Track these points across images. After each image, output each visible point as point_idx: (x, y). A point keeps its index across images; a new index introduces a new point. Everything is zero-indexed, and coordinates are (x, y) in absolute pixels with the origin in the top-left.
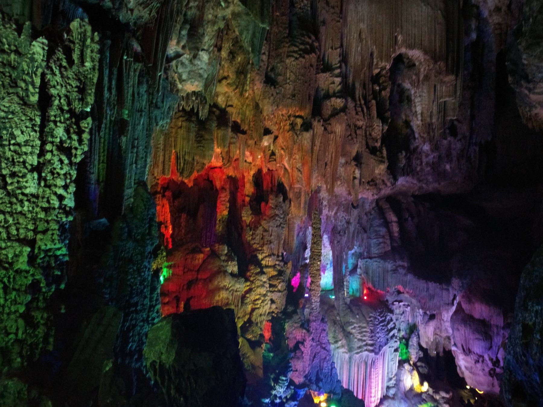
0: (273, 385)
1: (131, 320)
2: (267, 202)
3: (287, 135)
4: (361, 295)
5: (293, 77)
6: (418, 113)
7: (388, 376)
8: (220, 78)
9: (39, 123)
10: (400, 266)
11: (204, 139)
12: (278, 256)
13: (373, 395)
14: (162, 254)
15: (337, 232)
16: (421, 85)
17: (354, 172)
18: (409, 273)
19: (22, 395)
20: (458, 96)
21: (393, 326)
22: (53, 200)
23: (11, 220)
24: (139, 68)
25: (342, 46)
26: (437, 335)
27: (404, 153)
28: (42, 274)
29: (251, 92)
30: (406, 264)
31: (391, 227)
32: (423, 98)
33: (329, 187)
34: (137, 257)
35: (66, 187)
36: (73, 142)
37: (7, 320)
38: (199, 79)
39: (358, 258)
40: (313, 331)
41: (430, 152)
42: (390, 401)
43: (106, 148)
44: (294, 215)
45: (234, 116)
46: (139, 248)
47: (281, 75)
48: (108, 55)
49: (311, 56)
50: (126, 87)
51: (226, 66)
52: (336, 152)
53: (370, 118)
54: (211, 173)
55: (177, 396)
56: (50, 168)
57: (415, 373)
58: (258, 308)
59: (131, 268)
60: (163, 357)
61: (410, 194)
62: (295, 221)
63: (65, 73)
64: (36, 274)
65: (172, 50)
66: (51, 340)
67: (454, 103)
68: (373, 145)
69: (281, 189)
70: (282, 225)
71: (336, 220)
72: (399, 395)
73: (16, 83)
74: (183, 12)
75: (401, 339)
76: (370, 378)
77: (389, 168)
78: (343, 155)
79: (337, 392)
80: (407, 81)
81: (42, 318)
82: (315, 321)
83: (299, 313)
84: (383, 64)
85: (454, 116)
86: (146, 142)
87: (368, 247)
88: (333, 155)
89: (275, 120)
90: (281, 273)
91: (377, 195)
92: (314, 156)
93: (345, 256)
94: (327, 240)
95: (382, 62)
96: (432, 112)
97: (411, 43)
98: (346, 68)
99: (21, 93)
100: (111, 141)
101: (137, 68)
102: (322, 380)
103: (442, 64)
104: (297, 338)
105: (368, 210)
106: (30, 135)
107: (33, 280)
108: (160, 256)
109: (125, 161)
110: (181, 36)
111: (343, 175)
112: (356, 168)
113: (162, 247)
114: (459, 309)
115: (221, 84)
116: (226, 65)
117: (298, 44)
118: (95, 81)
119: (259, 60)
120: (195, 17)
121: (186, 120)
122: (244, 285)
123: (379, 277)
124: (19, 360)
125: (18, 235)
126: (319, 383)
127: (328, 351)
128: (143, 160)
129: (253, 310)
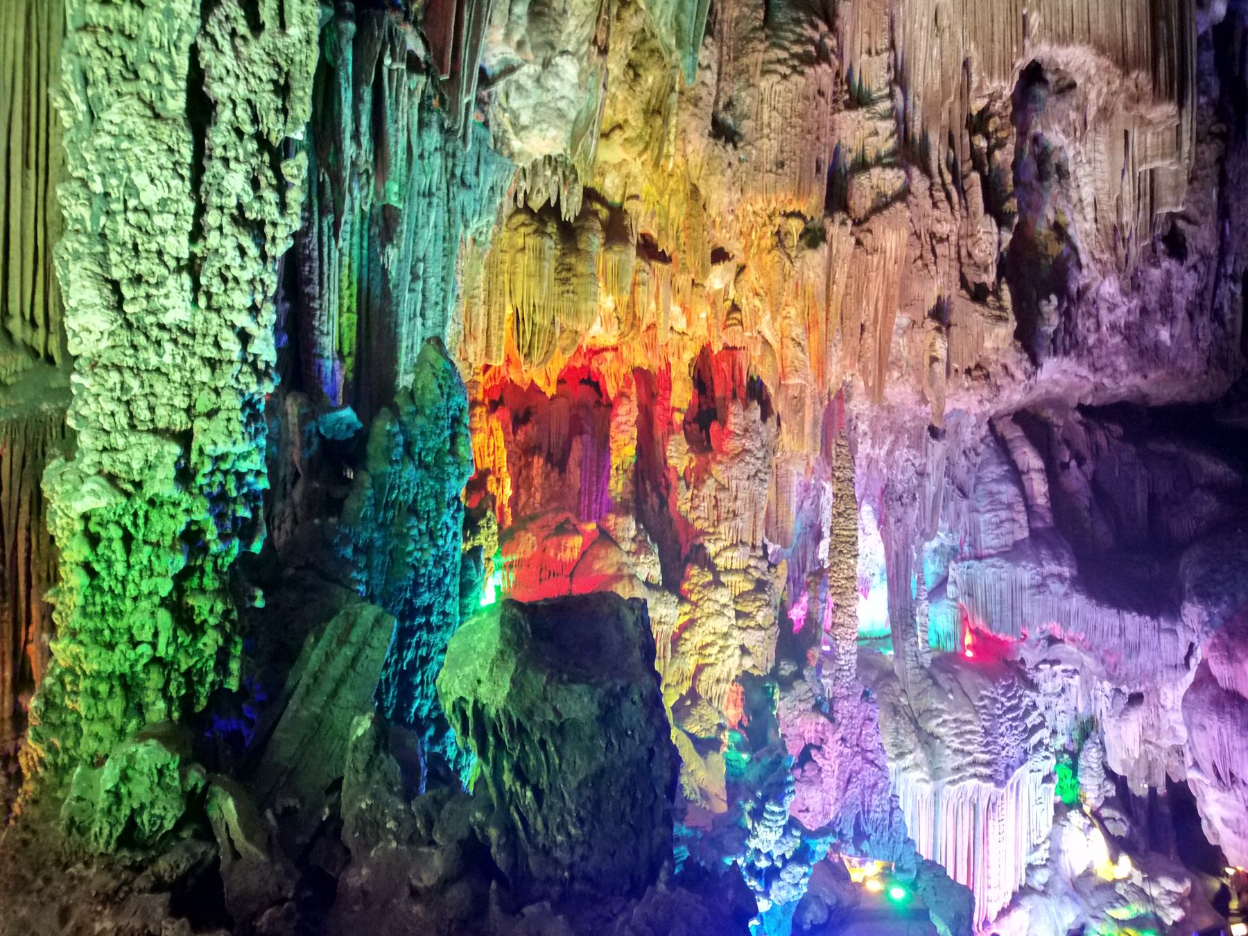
0: (750, 827)
1: (418, 646)
2: (724, 423)
3: (767, 259)
5: (777, 121)
6: (1085, 203)
8: (606, 127)
9: (189, 160)
10: (1052, 575)
11: (575, 275)
12: (754, 547)
13: (992, 882)
14: (489, 528)
16: (1091, 135)
17: (932, 345)
18: (1077, 591)
19: (168, 780)
20: (1185, 155)
22: (226, 340)
23: (134, 383)
24: (421, 87)
25: (892, 46)
26: (1150, 743)
27: (1054, 299)
28: (210, 511)
29: (679, 160)
30: (1067, 572)
31: (1026, 484)
32: (1098, 165)
33: (870, 384)
34: (427, 505)
35: (254, 310)
36: (267, 208)
37: (132, 613)
38: (558, 122)
40: (844, 722)
41: (1119, 299)
42: (1036, 898)
43: (355, 279)
44: (789, 454)
45: (642, 221)
46: (432, 483)
47: (749, 118)
48: (350, 57)
49: (819, 69)
51: (620, 97)
52: (888, 298)
54: (594, 365)
55: (518, 785)
56: (218, 265)
57: (1097, 833)
59: (413, 527)
61: (1074, 404)
62: (791, 468)
63: (243, 49)
64: (194, 509)
65: (494, 56)
66: (234, 666)
67: (1176, 173)
68: (977, 281)
69: (756, 392)
70: (761, 475)
71: (890, 467)
73: (136, 73)
75: (1059, 754)
76: (986, 842)
77: (1018, 335)
78: (904, 306)
79: (906, 867)
80: (1057, 127)
81: (211, 611)
82: (846, 698)
83: (807, 678)
84: (996, 84)
85: (1177, 205)
86: (444, 268)
87: (973, 534)
89: (737, 227)
90: (761, 586)
91: (989, 401)
92: (832, 309)
93: (915, 555)
94: (871, 516)
95: (991, 82)
96: (1119, 199)
97: (1064, 32)
98: (905, 99)
99: (147, 92)
100: (365, 262)
101: (416, 88)
102: (868, 837)
103: (1142, 77)
104: (806, 736)
105: (969, 445)
106: (169, 187)
107: (189, 524)
108: (484, 532)
109: (398, 305)
110: (514, 18)
111: (905, 354)
112: (938, 335)
113: (489, 513)
114: (1205, 678)
115: (610, 142)
116: (621, 93)
117: (787, 44)
118: (312, 68)
119: (694, 65)
121: (535, 232)
122: (678, 612)
123: (1001, 603)
124: (161, 705)
125: (152, 421)
126: (862, 841)
127: (880, 769)
128: (439, 308)
129: (700, 669)
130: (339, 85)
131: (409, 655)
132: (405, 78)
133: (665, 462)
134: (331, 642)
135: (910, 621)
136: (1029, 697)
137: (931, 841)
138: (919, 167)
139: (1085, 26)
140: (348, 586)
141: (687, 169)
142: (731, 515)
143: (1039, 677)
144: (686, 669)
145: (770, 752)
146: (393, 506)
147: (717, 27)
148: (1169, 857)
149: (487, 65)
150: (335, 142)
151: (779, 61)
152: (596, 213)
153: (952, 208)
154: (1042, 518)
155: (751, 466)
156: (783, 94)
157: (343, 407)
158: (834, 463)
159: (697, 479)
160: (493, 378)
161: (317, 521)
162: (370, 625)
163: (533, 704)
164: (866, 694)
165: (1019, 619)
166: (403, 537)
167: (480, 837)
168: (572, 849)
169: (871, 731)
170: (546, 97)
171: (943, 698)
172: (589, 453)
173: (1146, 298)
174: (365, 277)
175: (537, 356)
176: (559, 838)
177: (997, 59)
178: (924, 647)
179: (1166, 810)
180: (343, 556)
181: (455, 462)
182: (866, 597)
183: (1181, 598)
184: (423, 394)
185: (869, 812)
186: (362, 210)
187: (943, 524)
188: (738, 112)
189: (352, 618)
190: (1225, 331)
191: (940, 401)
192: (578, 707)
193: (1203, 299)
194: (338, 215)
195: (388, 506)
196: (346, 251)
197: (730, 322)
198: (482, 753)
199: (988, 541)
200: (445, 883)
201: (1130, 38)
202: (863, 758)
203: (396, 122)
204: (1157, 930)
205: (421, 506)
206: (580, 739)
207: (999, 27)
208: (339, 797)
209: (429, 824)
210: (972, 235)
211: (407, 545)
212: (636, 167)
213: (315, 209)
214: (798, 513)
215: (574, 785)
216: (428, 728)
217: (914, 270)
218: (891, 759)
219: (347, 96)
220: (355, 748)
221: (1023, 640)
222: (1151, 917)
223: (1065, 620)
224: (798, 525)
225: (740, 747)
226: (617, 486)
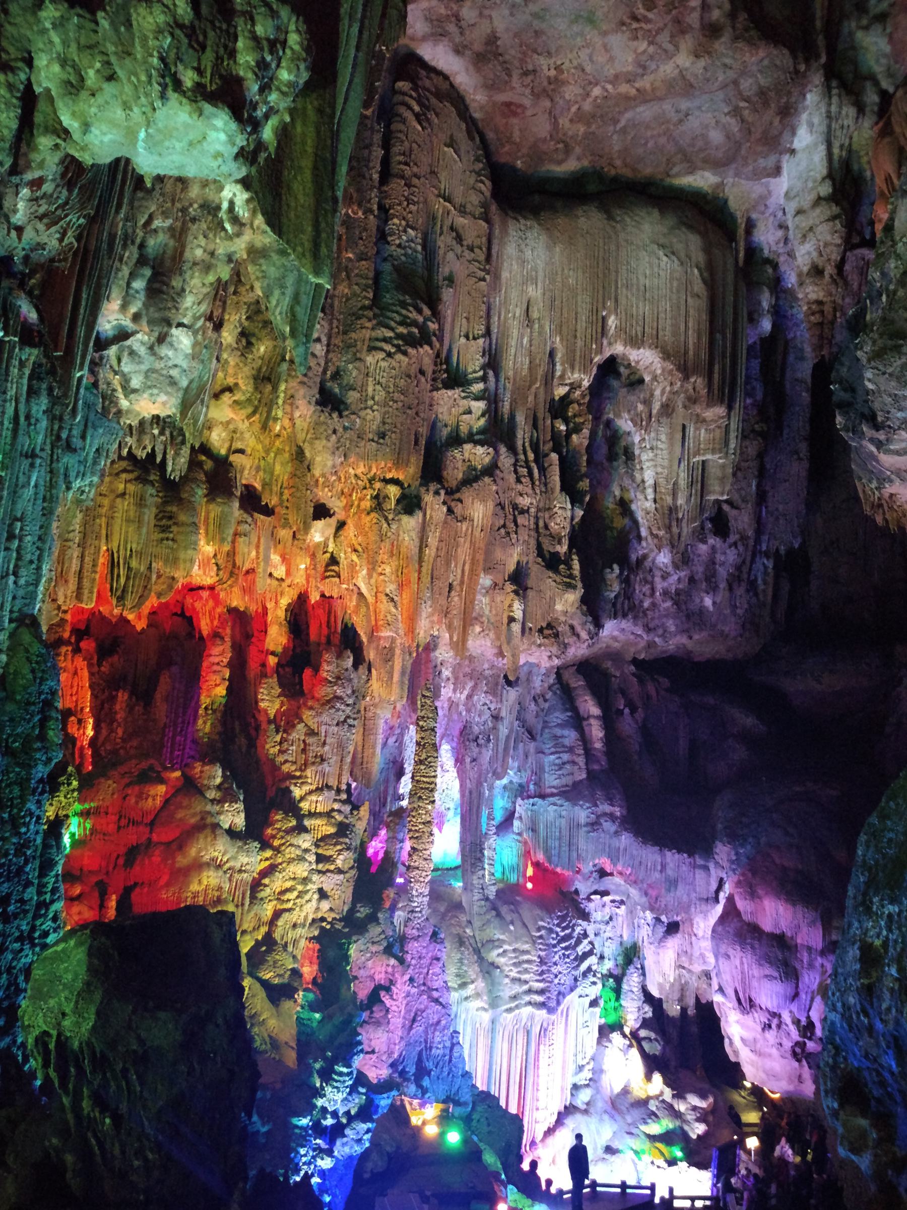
0: (318, 1085)
2: (317, 669)
3: (367, 520)
4: (521, 880)
5: (381, 395)
6: (647, 484)
8: (218, 388)
10: (605, 814)
11: (175, 524)
12: (339, 791)
13: (541, 1105)
14: (69, 784)
16: (654, 424)
17: (510, 606)
18: (626, 830)
21: (588, 948)
24: (33, 358)
25: (488, 333)
26: (684, 968)
29: (287, 423)
30: (617, 811)
31: (586, 729)
34: (11, 792)
38: (169, 389)
39: (516, 797)
41: (670, 569)
42: (578, 1117)
44: (377, 700)
46: (17, 769)
51: (232, 363)
52: (473, 563)
54: (189, 600)
55: (97, 1111)
57: (635, 1053)
60: (67, 1023)
61: (629, 658)
65: (109, 322)
67: (723, 466)
71: (468, 711)
72: (600, 1105)
74: (138, 241)
75: (605, 977)
76: (536, 1066)
77: (584, 600)
78: (488, 570)
79: (462, 1100)
80: (626, 416)
84: (576, 376)
85: (722, 494)
86: (41, 527)
87: (538, 772)
88: (467, 568)
90: (343, 829)
91: (558, 657)
92: (424, 570)
94: (449, 755)
95: (572, 373)
97: (637, 335)
98: (497, 381)
101: (27, 360)
102: (429, 1074)
103: (699, 381)
104: (377, 977)
111: (487, 612)
114: (731, 912)
116: (231, 359)
117: (393, 324)
119: (306, 354)
120: (164, 252)
121: (136, 479)
122: (259, 858)
127: (444, 1007)
128: (34, 566)
129: (277, 914)
132: (17, 350)
135: (479, 855)
136: (581, 926)
138: (506, 446)
141: (294, 432)
142: (318, 760)
143: (591, 907)
144: (263, 915)
148: (695, 1072)
151: (385, 340)
153: (533, 484)
154: (598, 761)
155: (341, 713)
165: (575, 854)
171: (505, 930)
176: (136, 1163)
177: (578, 354)
178: (490, 880)
179: (694, 1029)
181: (44, 747)
182: (440, 830)
183: (714, 838)
184: (14, 679)
185: (431, 1048)
187: (513, 763)
188: (345, 382)
190: (758, 599)
191: (515, 656)
201: (691, 347)
202: (429, 997)
207: (582, 324)
210: (549, 509)
212: (243, 426)
217: (498, 537)
221: (578, 872)
222: (679, 1131)
223: (614, 857)
225: (313, 1007)
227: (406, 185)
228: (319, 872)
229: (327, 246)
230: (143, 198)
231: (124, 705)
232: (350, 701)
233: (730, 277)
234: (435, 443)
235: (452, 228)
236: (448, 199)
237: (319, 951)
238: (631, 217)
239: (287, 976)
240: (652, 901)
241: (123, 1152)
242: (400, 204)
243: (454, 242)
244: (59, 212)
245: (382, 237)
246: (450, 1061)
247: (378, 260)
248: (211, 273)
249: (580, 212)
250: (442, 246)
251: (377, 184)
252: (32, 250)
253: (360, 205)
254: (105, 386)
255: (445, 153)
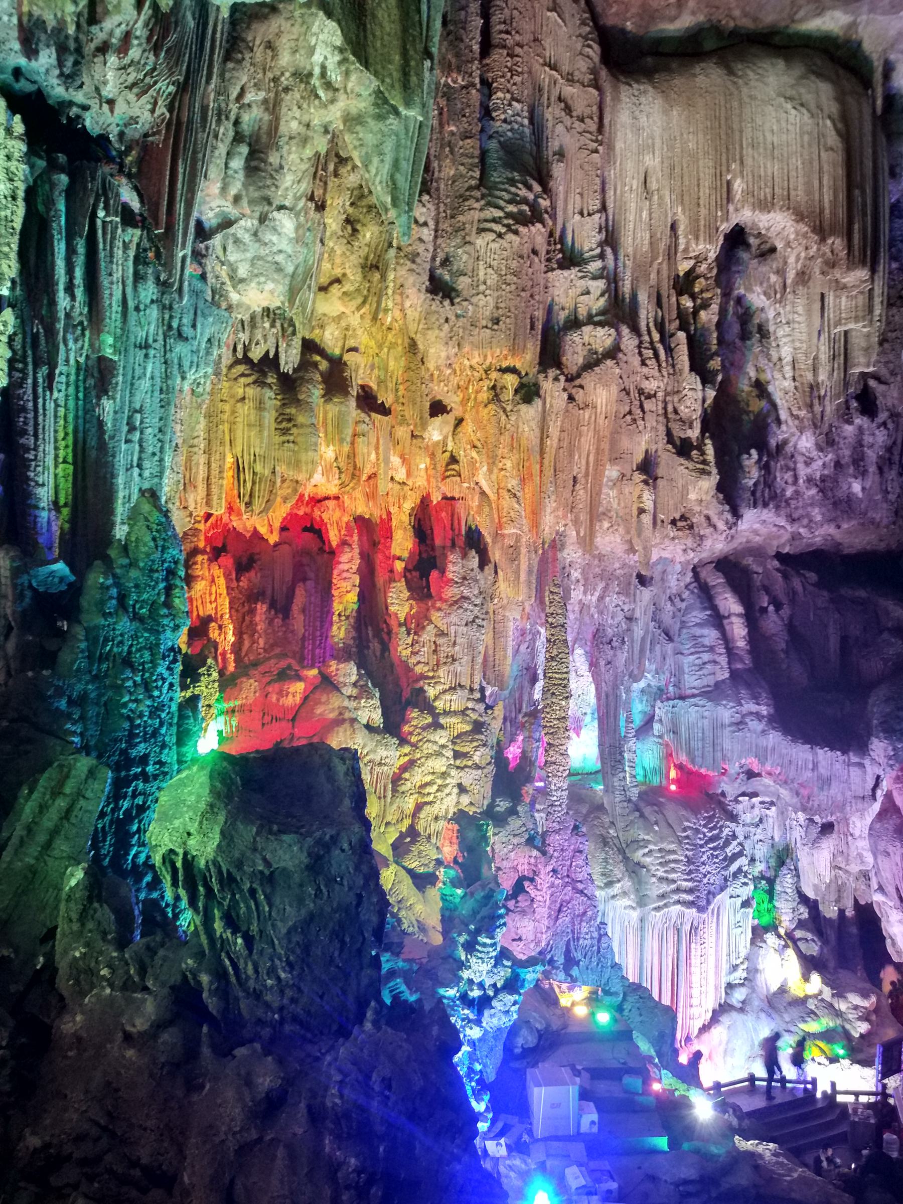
0: (463, 958)
1: (134, 795)
2: (443, 571)
3: (484, 412)
4: (664, 782)
5: (492, 279)
6: (784, 362)
7: (729, 961)
8: (324, 280)
10: (752, 713)
11: (294, 426)
12: (472, 690)
13: (695, 1002)
15: (604, 640)
17: (640, 497)
18: (774, 728)
21: (738, 849)
24: (136, 240)
25: (604, 208)
26: (840, 868)
29: (398, 314)
30: (764, 710)
31: (727, 628)
34: (141, 657)
38: (276, 276)
39: (655, 700)
40: (556, 854)
41: (814, 453)
42: (734, 1014)
43: (70, 429)
44: (505, 601)
46: (146, 635)
50: (106, 283)
51: (339, 252)
52: (598, 451)
53: (675, 373)
54: (317, 513)
57: (791, 953)
58: (430, 803)
59: (128, 679)
60: (192, 842)
65: (212, 209)
67: (868, 335)
68: (683, 436)
71: (601, 613)
72: (756, 1003)
74: (233, 117)
75: (755, 879)
76: (688, 965)
77: (720, 488)
78: (614, 460)
79: (613, 990)
80: (758, 289)
82: (557, 832)
85: (868, 366)
86: (161, 419)
87: (679, 674)
88: (592, 458)
89: (455, 381)
90: (478, 727)
91: (693, 550)
92: (546, 461)
94: (583, 659)
95: (697, 244)
97: (766, 198)
98: (616, 259)
100: (80, 413)
101: (131, 241)
103: (837, 243)
104: (520, 868)
105: (674, 591)
109: (114, 456)
110: (230, 172)
111: (615, 506)
113: (210, 661)
117: (502, 203)
118: (18, 224)
120: (260, 128)
121: (254, 382)
122: (398, 753)
127: (589, 898)
128: (157, 458)
129: (419, 807)
130: (53, 236)
131: (126, 804)
132: (119, 231)
133: (387, 609)
134: (44, 794)
135: (619, 757)
136: (729, 828)
137: (638, 963)
138: (629, 327)
139: (785, 193)
140: (62, 737)
142: (450, 660)
145: (483, 887)
146: (107, 659)
147: (434, 184)
149: (204, 218)
150: (48, 295)
151: (494, 220)
152: (315, 365)
153: (660, 366)
154: (741, 660)
156: (499, 252)
157: (55, 561)
158: (548, 610)
159: (418, 625)
160: (214, 526)
161: (30, 674)
162: (83, 776)
163: (243, 855)
164: (576, 827)
165: (719, 754)
166: (119, 689)
167: (192, 982)
168: (282, 992)
169: (580, 862)
170: (263, 251)
172: (313, 599)
173: (840, 452)
174: (81, 428)
175: (257, 506)
176: (269, 982)
177: (702, 223)
179: (854, 930)
180: (57, 708)
182: (578, 735)
183: (869, 735)
184: (137, 547)
185: (578, 939)
186: (77, 362)
188: (455, 268)
189: (66, 770)
191: (647, 550)
192: (287, 857)
193: (892, 454)
194: (53, 366)
195: (103, 658)
196: (62, 402)
197: (448, 473)
198: (193, 903)
199: (691, 681)
200: (159, 1026)
201: (827, 205)
203: (110, 275)
204: (845, 1042)
205: (136, 658)
206: (289, 886)
207: (705, 192)
208: (54, 946)
209: (143, 971)
211: (122, 697)
212: (354, 320)
213: (30, 360)
214: (514, 656)
215: (284, 931)
216: (146, 874)
218: (600, 888)
219: (60, 248)
220: (69, 899)
221: (723, 774)
222: (840, 1029)
223: (762, 755)
224: (515, 667)
225: (455, 883)
226: (340, 632)
227: (508, 55)
228: (458, 767)
229: (417, 75)
230: (234, 69)
231: (264, 617)
232: (478, 602)
233: (868, 127)
234: (553, 328)
235: (560, 99)
236: (554, 67)
237: (458, 831)
238: (753, 71)
239: (431, 865)
240: (804, 801)
241: (256, 971)
242: (503, 77)
243: (563, 113)
244: (148, 80)
245: (487, 113)
246: (599, 952)
247: (485, 137)
248: (308, 146)
249: (697, 70)
250: (550, 118)
251: (477, 56)
252: (125, 125)
253: (459, 71)
254: (214, 280)
255: (548, 18)
